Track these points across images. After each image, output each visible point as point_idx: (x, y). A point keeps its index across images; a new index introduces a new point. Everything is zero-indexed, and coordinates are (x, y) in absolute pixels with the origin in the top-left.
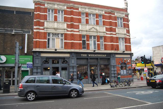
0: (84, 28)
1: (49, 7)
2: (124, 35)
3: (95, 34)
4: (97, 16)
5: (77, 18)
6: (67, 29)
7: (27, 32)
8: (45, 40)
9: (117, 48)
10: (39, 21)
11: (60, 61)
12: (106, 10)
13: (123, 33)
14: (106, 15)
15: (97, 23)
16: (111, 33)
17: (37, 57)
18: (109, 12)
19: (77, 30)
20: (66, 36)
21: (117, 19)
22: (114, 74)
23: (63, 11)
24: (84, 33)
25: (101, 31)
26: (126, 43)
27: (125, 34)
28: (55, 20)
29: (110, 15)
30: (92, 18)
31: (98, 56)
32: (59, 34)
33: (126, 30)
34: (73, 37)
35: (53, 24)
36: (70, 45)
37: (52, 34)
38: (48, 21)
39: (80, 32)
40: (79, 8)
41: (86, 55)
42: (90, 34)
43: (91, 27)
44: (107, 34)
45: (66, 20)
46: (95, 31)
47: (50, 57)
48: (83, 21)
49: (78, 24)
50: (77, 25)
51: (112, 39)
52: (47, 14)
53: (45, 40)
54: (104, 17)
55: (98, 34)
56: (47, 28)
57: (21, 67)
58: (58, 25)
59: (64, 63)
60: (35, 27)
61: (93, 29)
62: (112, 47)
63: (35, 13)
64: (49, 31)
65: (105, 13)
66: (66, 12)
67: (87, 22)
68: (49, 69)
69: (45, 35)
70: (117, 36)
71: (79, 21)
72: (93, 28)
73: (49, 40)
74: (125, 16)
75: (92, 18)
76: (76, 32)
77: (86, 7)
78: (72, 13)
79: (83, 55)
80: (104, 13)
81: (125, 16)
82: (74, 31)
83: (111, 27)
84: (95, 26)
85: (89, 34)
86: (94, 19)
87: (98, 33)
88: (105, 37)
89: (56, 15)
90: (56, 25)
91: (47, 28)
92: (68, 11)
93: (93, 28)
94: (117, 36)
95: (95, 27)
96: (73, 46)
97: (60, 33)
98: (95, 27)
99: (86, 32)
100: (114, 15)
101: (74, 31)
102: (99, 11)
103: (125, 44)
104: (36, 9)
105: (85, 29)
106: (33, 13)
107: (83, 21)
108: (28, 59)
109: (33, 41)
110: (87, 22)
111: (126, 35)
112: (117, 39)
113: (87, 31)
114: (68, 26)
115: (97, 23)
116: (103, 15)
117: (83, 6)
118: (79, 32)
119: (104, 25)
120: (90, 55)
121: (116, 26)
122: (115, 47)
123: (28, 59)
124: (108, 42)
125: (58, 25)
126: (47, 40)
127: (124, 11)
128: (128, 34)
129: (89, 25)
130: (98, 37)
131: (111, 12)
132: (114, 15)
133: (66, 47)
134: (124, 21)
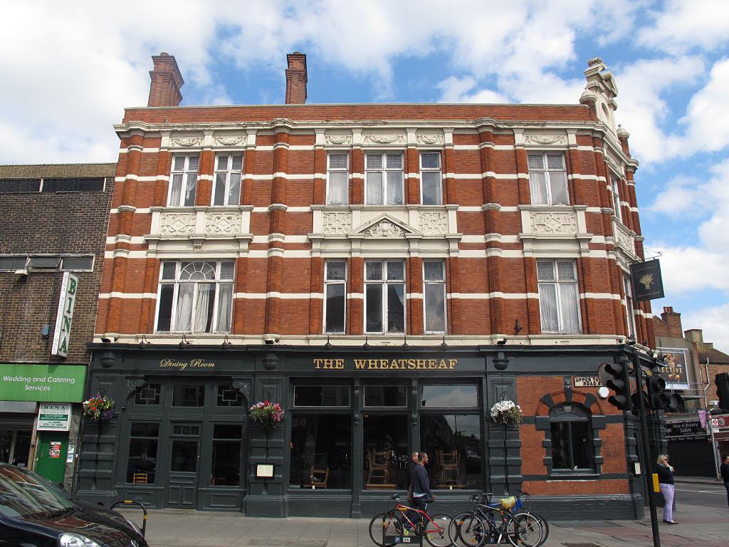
0: (336, 225)
1: (176, 146)
2: (574, 247)
3: (398, 251)
4: (406, 158)
5: (306, 181)
7: (69, 263)
8: (315, 295)
9: (529, 317)
11: (212, 394)
12: (462, 124)
13: (568, 232)
14: (465, 152)
15: (410, 196)
17: (498, 377)
19: (511, 239)
20: (240, 271)
22: (506, 466)
23: (227, 158)
24: (339, 251)
25: (428, 233)
26: (583, 289)
28: (352, 202)
30: (385, 175)
31: (406, 365)
32: (212, 263)
33: (588, 215)
34: (273, 273)
35: (188, 218)
36: (261, 313)
37: (182, 267)
38: (213, 210)
41: (339, 364)
42: (538, 251)
43: (374, 216)
44: (463, 246)
45: (576, 194)
46: (398, 235)
47: (464, 372)
48: (336, 192)
50: (305, 213)
51: (492, 273)
52: (419, 176)
53: (315, 295)
54: (448, 159)
55: (415, 251)
57: (36, 415)
58: (166, 223)
59: (226, 404)
60: (111, 240)
61: (386, 226)
62: (494, 316)
63: (118, 179)
64: (170, 252)
65: (458, 138)
67: (356, 194)
69: (151, 272)
70: (530, 251)
71: (315, 193)
72: (385, 220)
73: (167, 293)
74: (580, 143)
75: (385, 175)
76: (292, 249)
77: (348, 123)
78: (277, 160)
79: (322, 365)
80: (449, 138)
81: (580, 143)
82: (129, 247)
84: (399, 210)
85: (361, 251)
86: (394, 178)
88: (583, 266)
89: (412, 175)
90: (201, 224)
91: (323, 241)
92: (261, 152)
93: (385, 220)
95: (399, 216)
96: (270, 315)
97: (219, 259)
98: (399, 216)
104: (127, 163)
105: (341, 234)
106: (111, 179)
107: (336, 192)
108: (67, 380)
109: (97, 299)
110: (356, 194)
112: (527, 273)
114: (465, 224)
115: (410, 196)
118: (308, 245)
119: (448, 200)
120: (359, 364)
122: (515, 316)
123: (67, 380)
124: (470, 292)
125: (166, 223)
126: (157, 297)
127: (569, 118)
129: (362, 209)
130: (413, 264)
133: (239, 326)
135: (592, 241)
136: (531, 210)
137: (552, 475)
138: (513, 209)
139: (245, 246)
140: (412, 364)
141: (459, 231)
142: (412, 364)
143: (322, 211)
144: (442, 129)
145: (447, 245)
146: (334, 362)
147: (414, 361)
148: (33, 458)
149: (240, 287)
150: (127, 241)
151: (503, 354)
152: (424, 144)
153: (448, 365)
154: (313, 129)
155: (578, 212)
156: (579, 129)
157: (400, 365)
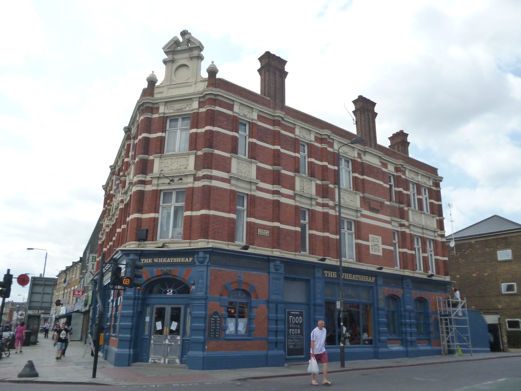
2: (354, 213)
6: (258, 181)
10: (278, 172)
16: (276, 188)
18: (274, 120)
19: (289, 192)
21: (302, 147)
22: (277, 320)
27: (251, 183)
29: (277, 128)
39: (233, 182)
40: (233, 105)
49: (291, 174)
56: (238, 179)
65: (260, 118)
66: (312, 151)
68: (70, 283)
80: (255, 116)
82: (283, 195)
83: (276, 168)
87: (425, 231)
88: (253, 200)
91: (238, 179)
94: (298, 204)
99: (420, 230)
100: (293, 132)
101: (283, 195)
102: (242, 107)
103: (355, 241)
111: (314, 203)
113: (423, 228)
114: (261, 174)
116: (252, 125)
117: (306, 126)
118: (228, 181)
121: (234, 150)
128: (440, 232)
131: (280, 119)
132: (293, 132)
134: (430, 198)
135: (258, 185)
136: (238, 158)
137: (372, 280)
138: (291, 174)
139: (254, 187)
140: (175, 260)
141: (257, 178)
142: (175, 260)
143: (237, 159)
144: (252, 108)
145: (250, 185)
146: (148, 260)
147: (176, 259)
148: (238, 309)
149: (190, 207)
150: (209, 174)
151: (202, 253)
152: (242, 115)
153: (189, 260)
154: (233, 101)
155: (312, 181)
156: (260, 111)
157: (170, 260)
